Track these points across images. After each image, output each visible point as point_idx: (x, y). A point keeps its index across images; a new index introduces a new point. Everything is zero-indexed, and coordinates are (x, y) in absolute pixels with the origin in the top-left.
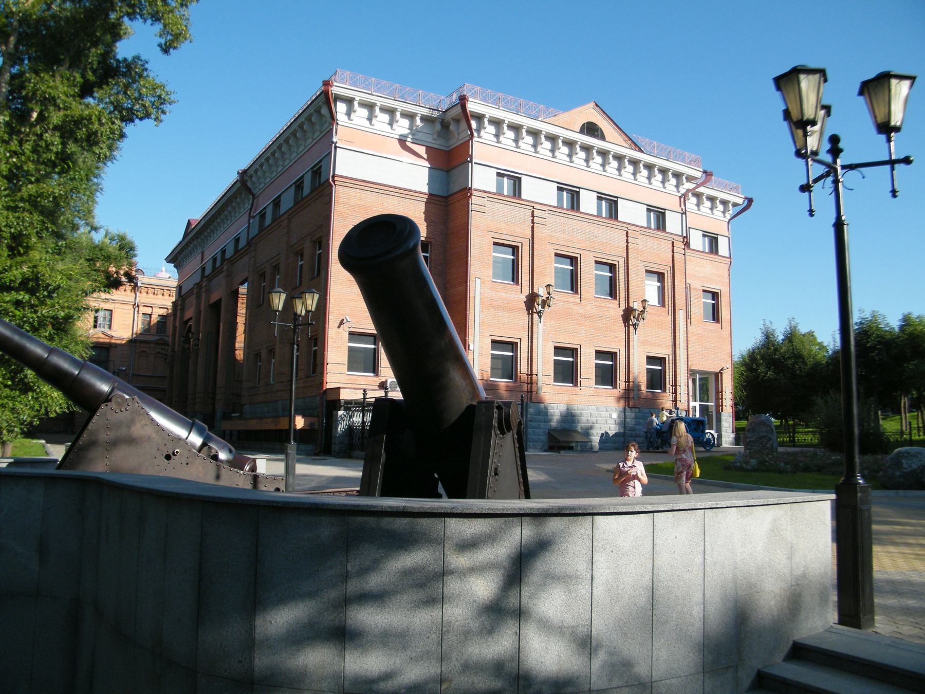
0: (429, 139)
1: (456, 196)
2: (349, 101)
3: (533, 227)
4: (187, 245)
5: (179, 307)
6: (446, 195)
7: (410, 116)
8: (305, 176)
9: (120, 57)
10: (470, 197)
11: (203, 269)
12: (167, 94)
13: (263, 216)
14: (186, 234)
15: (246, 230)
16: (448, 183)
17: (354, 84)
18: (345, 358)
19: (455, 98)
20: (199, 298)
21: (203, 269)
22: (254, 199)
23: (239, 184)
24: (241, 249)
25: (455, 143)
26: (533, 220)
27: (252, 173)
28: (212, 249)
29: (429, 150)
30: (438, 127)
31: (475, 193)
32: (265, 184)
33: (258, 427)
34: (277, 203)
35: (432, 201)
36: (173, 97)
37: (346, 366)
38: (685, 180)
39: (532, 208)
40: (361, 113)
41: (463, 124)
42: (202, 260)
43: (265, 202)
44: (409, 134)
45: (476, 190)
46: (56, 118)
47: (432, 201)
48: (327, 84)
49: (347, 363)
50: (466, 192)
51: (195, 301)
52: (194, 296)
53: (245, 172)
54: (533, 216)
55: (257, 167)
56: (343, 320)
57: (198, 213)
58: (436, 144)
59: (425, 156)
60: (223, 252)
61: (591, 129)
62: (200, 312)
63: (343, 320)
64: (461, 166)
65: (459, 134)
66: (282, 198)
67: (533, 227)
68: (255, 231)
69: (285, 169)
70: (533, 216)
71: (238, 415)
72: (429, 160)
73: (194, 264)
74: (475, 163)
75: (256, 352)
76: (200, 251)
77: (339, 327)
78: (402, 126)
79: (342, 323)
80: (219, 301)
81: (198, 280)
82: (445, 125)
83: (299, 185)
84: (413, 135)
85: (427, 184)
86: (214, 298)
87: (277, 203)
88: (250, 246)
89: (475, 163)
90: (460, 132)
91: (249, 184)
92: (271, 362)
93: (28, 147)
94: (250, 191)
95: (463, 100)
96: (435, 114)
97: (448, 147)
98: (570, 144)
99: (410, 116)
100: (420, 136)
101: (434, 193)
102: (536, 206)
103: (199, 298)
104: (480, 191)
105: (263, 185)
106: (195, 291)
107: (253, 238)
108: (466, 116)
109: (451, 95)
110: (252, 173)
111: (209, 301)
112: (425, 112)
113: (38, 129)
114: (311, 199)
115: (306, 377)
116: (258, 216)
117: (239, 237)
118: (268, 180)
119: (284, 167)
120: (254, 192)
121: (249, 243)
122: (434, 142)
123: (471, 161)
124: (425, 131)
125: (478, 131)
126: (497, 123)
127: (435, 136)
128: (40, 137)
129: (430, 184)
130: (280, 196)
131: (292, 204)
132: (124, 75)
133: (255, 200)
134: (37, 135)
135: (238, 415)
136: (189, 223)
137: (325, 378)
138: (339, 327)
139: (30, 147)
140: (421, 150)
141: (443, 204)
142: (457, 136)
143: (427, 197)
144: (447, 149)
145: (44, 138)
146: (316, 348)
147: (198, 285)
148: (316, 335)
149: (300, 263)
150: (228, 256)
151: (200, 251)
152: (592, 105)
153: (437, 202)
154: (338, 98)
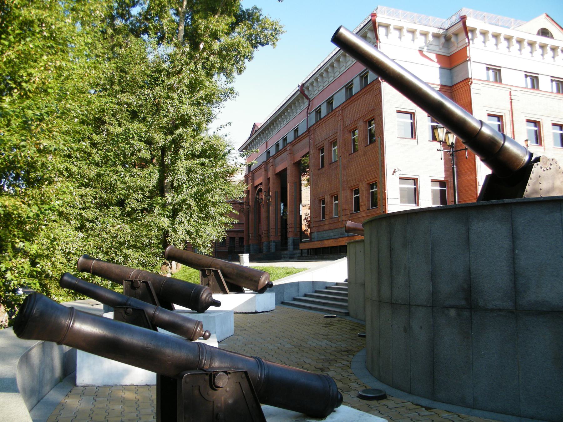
0: (437, 49)
1: (459, 85)
2: (387, 27)
3: (511, 102)
4: (251, 142)
5: (250, 178)
6: (450, 85)
7: (425, 34)
8: (354, 80)
9: (244, 8)
10: (471, 84)
11: (268, 152)
12: (280, 27)
13: (318, 112)
14: (252, 135)
15: (306, 120)
16: (452, 78)
17: (389, 15)
18: (398, 195)
19: (455, 19)
20: (266, 170)
21: (268, 152)
22: (310, 101)
23: (299, 93)
24: (301, 135)
25: (455, 49)
26: (511, 98)
27: (309, 85)
28: (275, 138)
29: (438, 56)
30: (443, 40)
31: (474, 81)
32: (319, 91)
33: (335, 245)
34: (330, 102)
35: (443, 90)
36: (283, 29)
37: (399, 200)
38: (435, 124)
39: (509, 90)
40: (394, 34)
41: (464, 34)
42: (267, 147)
43: (320, 102)
44: (424, 46)
45: (475, 79)
46: (216, 46)
47: (443, 90)
48: (374, 15)
49: (399, 198)
50: (467, 81)
51: (263, 173)
52: (263, 169)
53: (303, 85)
54: (511, 95)
55: (313, 80)
56: (395, 170)
57: (262, 119)
58: (443, 52)
59: (436, 60)
60: (285, 139)
61: (544, 32)
62: (269, 179)
63: (395, 170)
64: (458, 66)
65: (458, 43)
66: (335, 97)
67: (511, 102)
68: (313, 121)
69: (335, 79)
70: (511, 95)
71: (309, 239)
72: (438, 62)
73: (260, 150)
74: (473, 62)
75: (368, 182)
76: (264, 141)
77: (393, 174)
78: (420, 41)
79: (394, 172)
80: (285, 170)
81: (265, 159)
82: (448, 39)
83: (349, 87)
84: (428, 47)
85: (439, 78)
86: (279, 169)
87: (330, 102)
88: (309, 132)
89: (473, 62)
90: (459, 41)
91: (306, 92)
92: (333, 203)
93: (199, 66)
94: (307, 98)
95: (463, 19)
96: (441, 31)
97: (449, 54)
98: (531, 44)
99: (425, 34)
100: (431, 47)
101: (444, 84)
102: (512, 88)
103: (266, 170)
104: (477, 80)
105: (316, 92)
106: (263, 166)
107: (310, 127)
108: (466, 29)
109: (451, 18)
110: (309, 85)
111: (275, 171)
112: (436, 31)
113: (205, 55)
114: (360, 95)
115: (368, 210)
116: (315, 112)
117: (298, 128)
118: (321, 88)
119: (334, 77)
120: (310, 97)
121: (309, 130)
122: (440, 51)
123: (470, 60)
124: (434, 44)
125: (472, 39)
126: (484, 33)
127: (441, 47)
128: (208, 59)
129: (441, 77)
130: (333, 96)
131: (344, 100)
132: (248, 19)
133: (311, 103)
134: (205, 58)
135: (309, 239)
136: (255, 125)
137: (387, 208)
138: (393, 174)
139: (200, 67)
140: (433, 56)
141: (446, 91)
142: (456, 45)
143: (439, 87)
144: (449, 55)
145: (210, 59)
146: (337, 202)
147: (266, 163)
148: (376, 181)
149: (353, 138)
150: (289, 141)
151: (264, 141)
152: (544, 16)
153: (446, 91)
154: (381, 25)
